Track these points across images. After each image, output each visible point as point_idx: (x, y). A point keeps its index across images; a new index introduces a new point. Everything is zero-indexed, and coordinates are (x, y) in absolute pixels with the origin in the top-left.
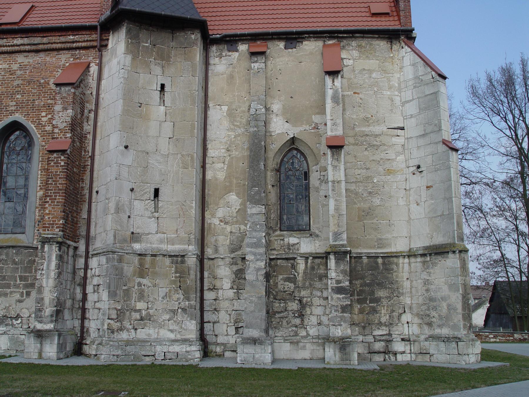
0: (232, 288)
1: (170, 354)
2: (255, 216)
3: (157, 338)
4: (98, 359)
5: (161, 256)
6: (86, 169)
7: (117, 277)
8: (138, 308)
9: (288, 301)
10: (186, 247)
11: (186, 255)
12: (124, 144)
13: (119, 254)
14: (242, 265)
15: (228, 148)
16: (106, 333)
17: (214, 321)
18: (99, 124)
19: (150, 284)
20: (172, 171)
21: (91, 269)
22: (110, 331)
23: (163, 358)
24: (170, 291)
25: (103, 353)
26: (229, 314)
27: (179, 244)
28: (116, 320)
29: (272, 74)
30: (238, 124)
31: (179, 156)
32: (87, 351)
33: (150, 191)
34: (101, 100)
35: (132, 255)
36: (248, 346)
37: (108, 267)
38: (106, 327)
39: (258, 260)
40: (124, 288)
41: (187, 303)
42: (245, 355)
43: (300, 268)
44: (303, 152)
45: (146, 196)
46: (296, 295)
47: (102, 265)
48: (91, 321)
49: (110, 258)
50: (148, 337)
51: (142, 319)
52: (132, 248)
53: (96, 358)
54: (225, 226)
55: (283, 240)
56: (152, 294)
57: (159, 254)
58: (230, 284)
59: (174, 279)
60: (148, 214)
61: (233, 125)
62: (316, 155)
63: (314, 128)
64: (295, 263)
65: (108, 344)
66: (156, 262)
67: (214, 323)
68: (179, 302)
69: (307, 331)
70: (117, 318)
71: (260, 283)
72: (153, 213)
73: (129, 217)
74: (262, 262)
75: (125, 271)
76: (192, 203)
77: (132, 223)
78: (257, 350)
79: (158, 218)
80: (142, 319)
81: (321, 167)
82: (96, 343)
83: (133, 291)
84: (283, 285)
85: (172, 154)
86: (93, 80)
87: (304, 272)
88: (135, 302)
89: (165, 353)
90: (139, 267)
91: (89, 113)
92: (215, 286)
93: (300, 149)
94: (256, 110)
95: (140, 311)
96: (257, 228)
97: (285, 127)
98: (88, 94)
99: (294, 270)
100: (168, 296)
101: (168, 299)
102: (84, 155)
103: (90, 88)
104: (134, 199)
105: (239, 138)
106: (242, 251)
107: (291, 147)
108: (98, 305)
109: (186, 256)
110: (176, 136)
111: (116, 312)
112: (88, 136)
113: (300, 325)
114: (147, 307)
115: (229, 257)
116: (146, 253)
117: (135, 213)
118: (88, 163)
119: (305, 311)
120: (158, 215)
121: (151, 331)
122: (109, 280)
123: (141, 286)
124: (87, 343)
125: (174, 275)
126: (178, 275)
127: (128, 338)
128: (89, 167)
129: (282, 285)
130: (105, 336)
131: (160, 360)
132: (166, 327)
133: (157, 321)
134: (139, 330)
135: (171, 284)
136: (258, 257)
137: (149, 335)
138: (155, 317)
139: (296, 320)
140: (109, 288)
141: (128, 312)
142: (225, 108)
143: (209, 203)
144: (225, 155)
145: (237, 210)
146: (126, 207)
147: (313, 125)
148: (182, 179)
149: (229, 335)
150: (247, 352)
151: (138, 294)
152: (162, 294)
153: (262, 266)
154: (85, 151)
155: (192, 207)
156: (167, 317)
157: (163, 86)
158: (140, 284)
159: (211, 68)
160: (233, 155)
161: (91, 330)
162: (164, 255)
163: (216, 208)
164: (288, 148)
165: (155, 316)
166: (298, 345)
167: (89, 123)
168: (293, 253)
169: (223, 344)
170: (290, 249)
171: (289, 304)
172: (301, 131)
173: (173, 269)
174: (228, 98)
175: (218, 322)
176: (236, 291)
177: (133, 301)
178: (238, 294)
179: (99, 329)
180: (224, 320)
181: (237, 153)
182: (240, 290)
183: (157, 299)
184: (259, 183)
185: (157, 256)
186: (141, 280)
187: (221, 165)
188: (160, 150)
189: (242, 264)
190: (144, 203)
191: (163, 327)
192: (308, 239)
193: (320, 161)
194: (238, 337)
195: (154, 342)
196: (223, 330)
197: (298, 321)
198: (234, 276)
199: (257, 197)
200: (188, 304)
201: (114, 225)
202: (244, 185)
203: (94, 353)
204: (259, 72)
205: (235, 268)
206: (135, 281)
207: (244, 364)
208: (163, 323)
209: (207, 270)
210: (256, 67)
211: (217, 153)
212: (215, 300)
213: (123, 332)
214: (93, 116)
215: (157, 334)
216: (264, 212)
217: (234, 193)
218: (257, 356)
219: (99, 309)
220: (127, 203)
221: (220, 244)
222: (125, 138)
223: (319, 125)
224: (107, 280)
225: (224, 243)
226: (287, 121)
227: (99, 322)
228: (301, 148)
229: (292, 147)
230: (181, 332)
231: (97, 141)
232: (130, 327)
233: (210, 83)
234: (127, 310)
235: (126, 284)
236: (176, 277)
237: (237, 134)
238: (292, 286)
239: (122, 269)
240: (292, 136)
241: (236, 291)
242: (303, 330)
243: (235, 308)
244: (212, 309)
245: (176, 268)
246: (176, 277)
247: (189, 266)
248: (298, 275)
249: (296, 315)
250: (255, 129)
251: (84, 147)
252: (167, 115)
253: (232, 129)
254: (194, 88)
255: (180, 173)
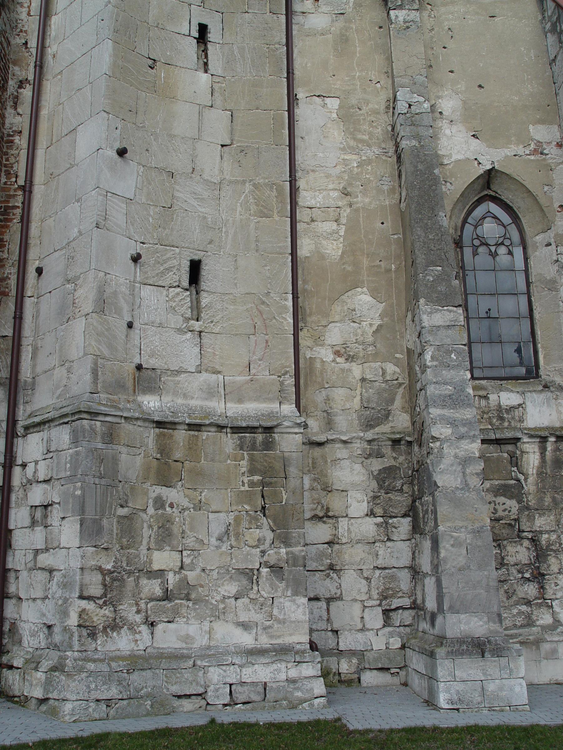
0: (371, 514)
1: (246, 688)
2: (443, 333)
3: (209, 648)
4: (54, 713)
5: (213, 429)
6: (11, 216)
7: (103, 482)
8: (156, 567)
9: (505, 542)
10: (275, 406)
11: (276, 426)
12: (117, 145)
13: (108, 419)
14: (395, 458)
15: (345, 188)
16: (76, 638)
17: (328, 596)
18: (44, 113)
19: (185, 503)
20: (231, 221)
21: (24, 465)
22: (85, 632)
23: (227, 700)
24: (237, 520)
25: (69, 696)
26: (367, 579)
27: (257, 399)
28: (101, 602)
29: (432, 37)
30: (364, 137)
31: (248, 187)
32: (16, 687)
33: (180, 265)
34: (49, 58)
35: (139, 423)
36: (466, 661)
37: (77, 453)
38: (73, 620)
39: (461, 437)
40: (122, 512)
41: (283, 551)
42: (460, 687)
43: (528, 464)
44: (511, 204)
45: (170, 278)
46: (523, 527)
47: (57, 451)
48: (25, 604)
49: (84, 430)
50: (184, 645)
51: (167, 596)
52: (140, 406)
53: (44, 708)
54: (347, 366)
55: (486, 397)
56: (192, 529)
57: (207, 422)
58: (365, 503)
59: (246, 488)
60: (176, 321)
61: (355, 139)
62: (545, 209)
63: (535, 152)
64: (518, 452)
65: (81, 670)
66: (200, 444)
67: (329, 600)
68: (262, 548)
69: (554, 614)
70: (105, 595)
71: (473, 495)
72: (187, 320)
73: (130, 325)
74: (473, 441)
75: (122, 466)
76: (286, 300)
77: (137, 342)
78: (490, 671)
79: (200, 332)
80: (167, 596)
81: (557, 235)
82: (45, 665)
83: (143, 521)
84: (493, 505)
85: (231, 182)
86: (29, 14)
87: (540, 473)
88: (148, 549)
89: (231, 685)
90: (159, 456)
91: (20, 87)
92: (328, 510)
93: (503, 198)
94: (410, 106)
95: (161, 573)
96: (452, 360)
97: (472, 148)
98: (18, 45)
99: (515, 469)
100: (232, 534)
101: (233, 542)
102: (5, 183)
103: (21, 31)
104: (140, 283)
105: (369, 168)
106: (391, 424)
107: (482, 194)
108: (45, 560)
109: (276, 430)
110: (238, 141)
111: (100, 577)
112: (17, 139)
113: (536, 598)
114: (179, 564)
115: (361, 438)
116: (177, 420)
117: (145, 318)
118: (17, 201)
119: (545, 566)
120: (200, 327)
121: (193, 629)
122: (82, 488)
123: (162, 506)
124: (15, 665)
125: (246, 480)
126: (257, 478)
127: (133, 650)
128: (18, 211)
129: (490, 503)
130: (71, 647)
131: (220, 707)
132: (230, 617)
133: (207, 601)
134: (160, 628)
135: (240, 502)
136: (463, 430)
137: (187, 638)
138: (200, 590)
139: (526, 586)
140: (82, 511)
141: (132, 579)
142: (333, 104)
143: (308, 311)
144: (340, 204)
145: (374, 328)
146: (122, 300)
147: (532, 146)
148: (257, 241)
149: (368, 630)
150: (465, 676)
151: (155, 528)
152: (217, 529)
153: (475, 454)
154: (8, 174)
155: (285, 307)
156: (232, 588)
157: (203, 29)
158: (159, 503)
159: (296, 19)
160: (357, 203)
161: (25, 629)
162: (221, 428)
163: (324, 323)
164: (476, 195)
165: (202, 586)
166: (538, 648)
167: (20, 110)
168: (510, 428)
169: (352, 653)
170: (502, 419)
171: (509, 548)
172: (507, 157)
173: (244, 463)
174: (339, 82)
175: (340, 598)
176: (380, 520)
177: (143, 549)
178: (386, 527)
179: (49, 627)
180: (355, 594)
181: (367, 200)
182: (391, 517)
183: (206, 541)
184: (443, 257)
185: (203, 428)
186: (164, 491)
187: (329, 226)
188: (202, 170)
189: (394, 455)
190: (165, 293)
191: (222, 617)
192: (542, 396)
193: (553, 222)
194: (391, 635)
195: (203, 657)
196: (352, 618)
197: (531, 590)
198: (374, 484)
199: (442, 288)
200: (287, 553)
201: (93, 343)
202: (389, 271)
203: (38, 693)
204: (408, 28)
205: (377, 465)
206: (146, 493)
207: (458, 710)
208: (221, 606)
209: (309, 471)
210: (401, 19)
211: (320, 198)
212: (330, 543)
213: (119, 633)
214: (30, 94)
215: (207, 636)
216: (462, 323)
217: (365, 289)
218: (491, 687)
219: (51, 571)
220: (123, 289)
221: (337, 407)
222: (118, 132)
223: (545, 146)
224: (75, 489)
225: (348, 406)
226: (473, 136)
227: (49, 607)
228: (506, 196)
229: (485, 192)
230: (270, 627)
231: (40, 153)
232: (138, 618)
233: (296, 51)
234: (130, 573)
235: (126, 502)
236: (252, 484)
237: (364, 158)
238: (513, 504)
239: (115, 460)
240: (489, 167)
241: (380, 520)
242: (545, 612)
243: (380, 562)
244: (322, 565)
245: (252, 459)
246: (252, 484)
247: (286, 454)
248: (526, 479)
249: (527, 575)
250: (414, 143)
251: (6, 166)
252: (216, 94)
253: (352, 148)
254: (277, 39)
255: (252, 225)
